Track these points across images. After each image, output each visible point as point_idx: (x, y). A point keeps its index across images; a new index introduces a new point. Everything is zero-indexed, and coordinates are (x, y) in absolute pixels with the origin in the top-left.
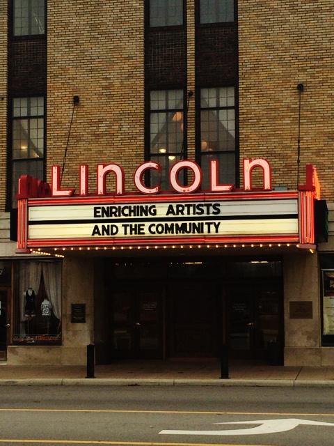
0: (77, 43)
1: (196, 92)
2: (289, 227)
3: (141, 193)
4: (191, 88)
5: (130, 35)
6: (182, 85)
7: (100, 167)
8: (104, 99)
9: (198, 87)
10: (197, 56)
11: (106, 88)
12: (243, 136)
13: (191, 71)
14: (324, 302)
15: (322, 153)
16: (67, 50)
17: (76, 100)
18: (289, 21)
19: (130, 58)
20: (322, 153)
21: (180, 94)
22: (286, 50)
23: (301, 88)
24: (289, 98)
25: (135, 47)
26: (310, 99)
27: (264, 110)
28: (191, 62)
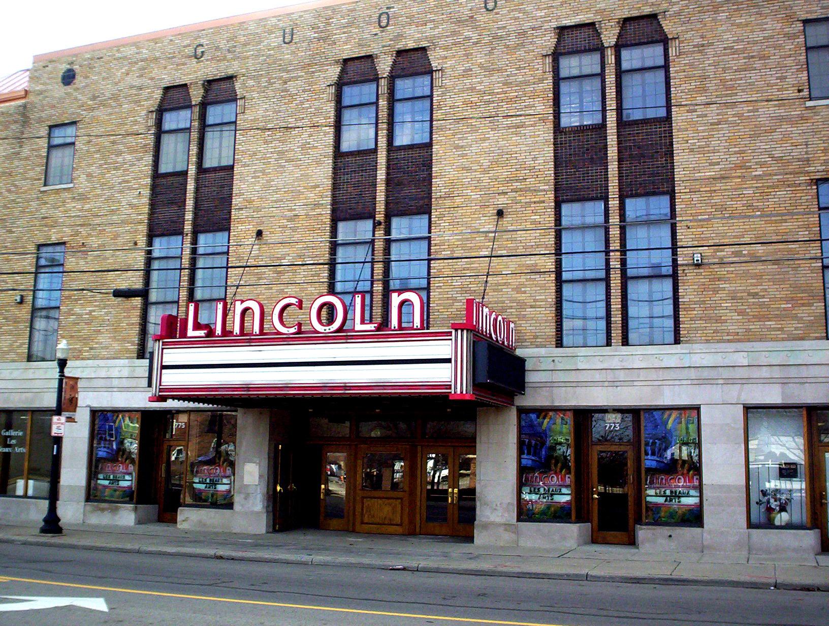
0: (263, 172)
1: (385, 222)
2: (440, 374)
3: (279, 333)
4: (380, 217)
5: (318, 163)
6: (371, 215)
7: (238, 303)
8: (288, 232)
9: (388, 217)
10: (388, 182)
11: (290, 219)
12: (435, 271)
13: (381, 197)
14: (703, 433)
15: (523, 289)
16: (253, 180)
17: (259, 234)
18: (488, 138)
19: (317, 186)
20: (523, 289)
21: (369, 224)
22: (485, 172)
23: (500, 213)
24: (488, 224)
25: (323, 174)
26: (506, 222)
27: (458, 240)
28: (381, 189)
